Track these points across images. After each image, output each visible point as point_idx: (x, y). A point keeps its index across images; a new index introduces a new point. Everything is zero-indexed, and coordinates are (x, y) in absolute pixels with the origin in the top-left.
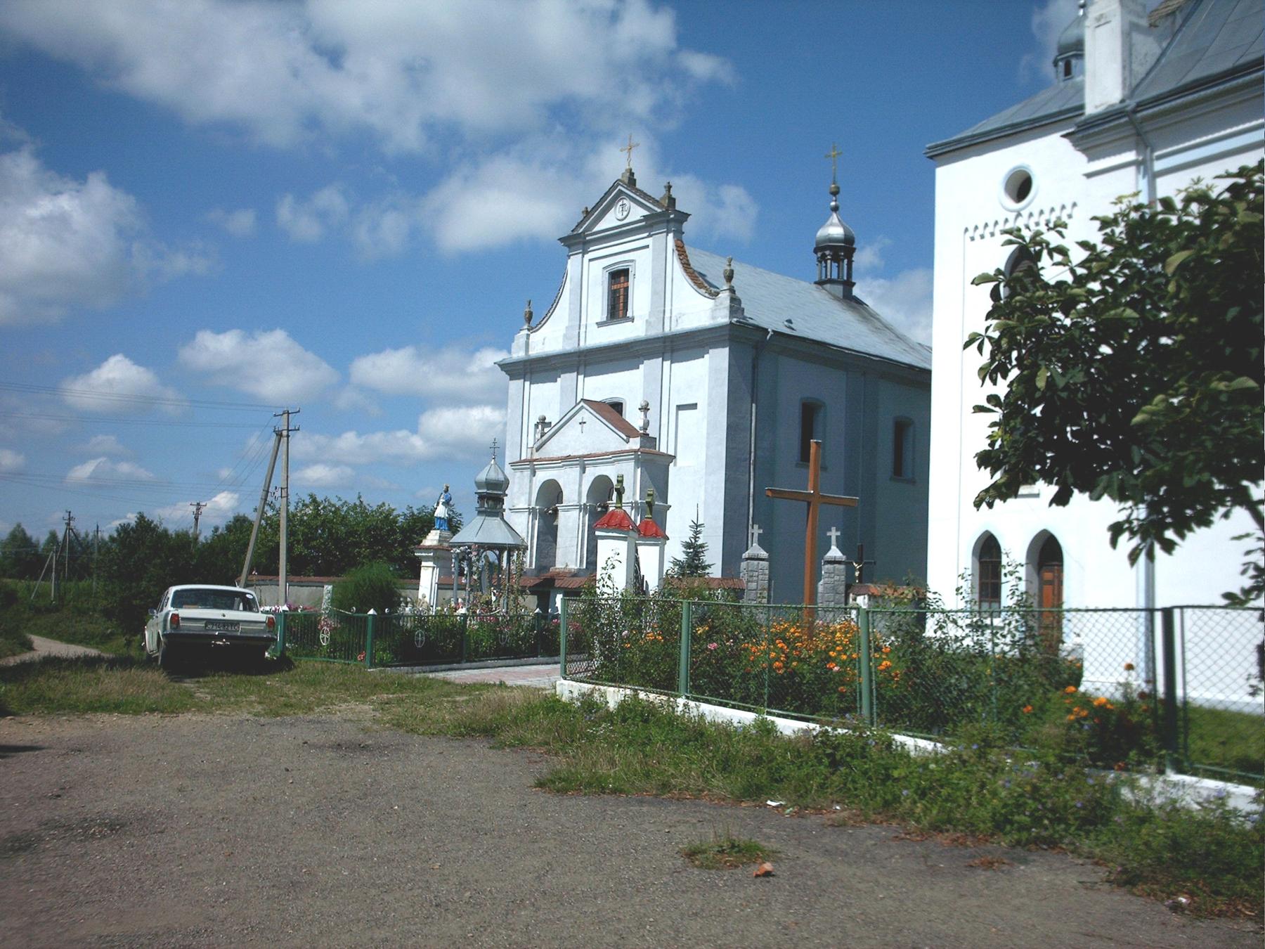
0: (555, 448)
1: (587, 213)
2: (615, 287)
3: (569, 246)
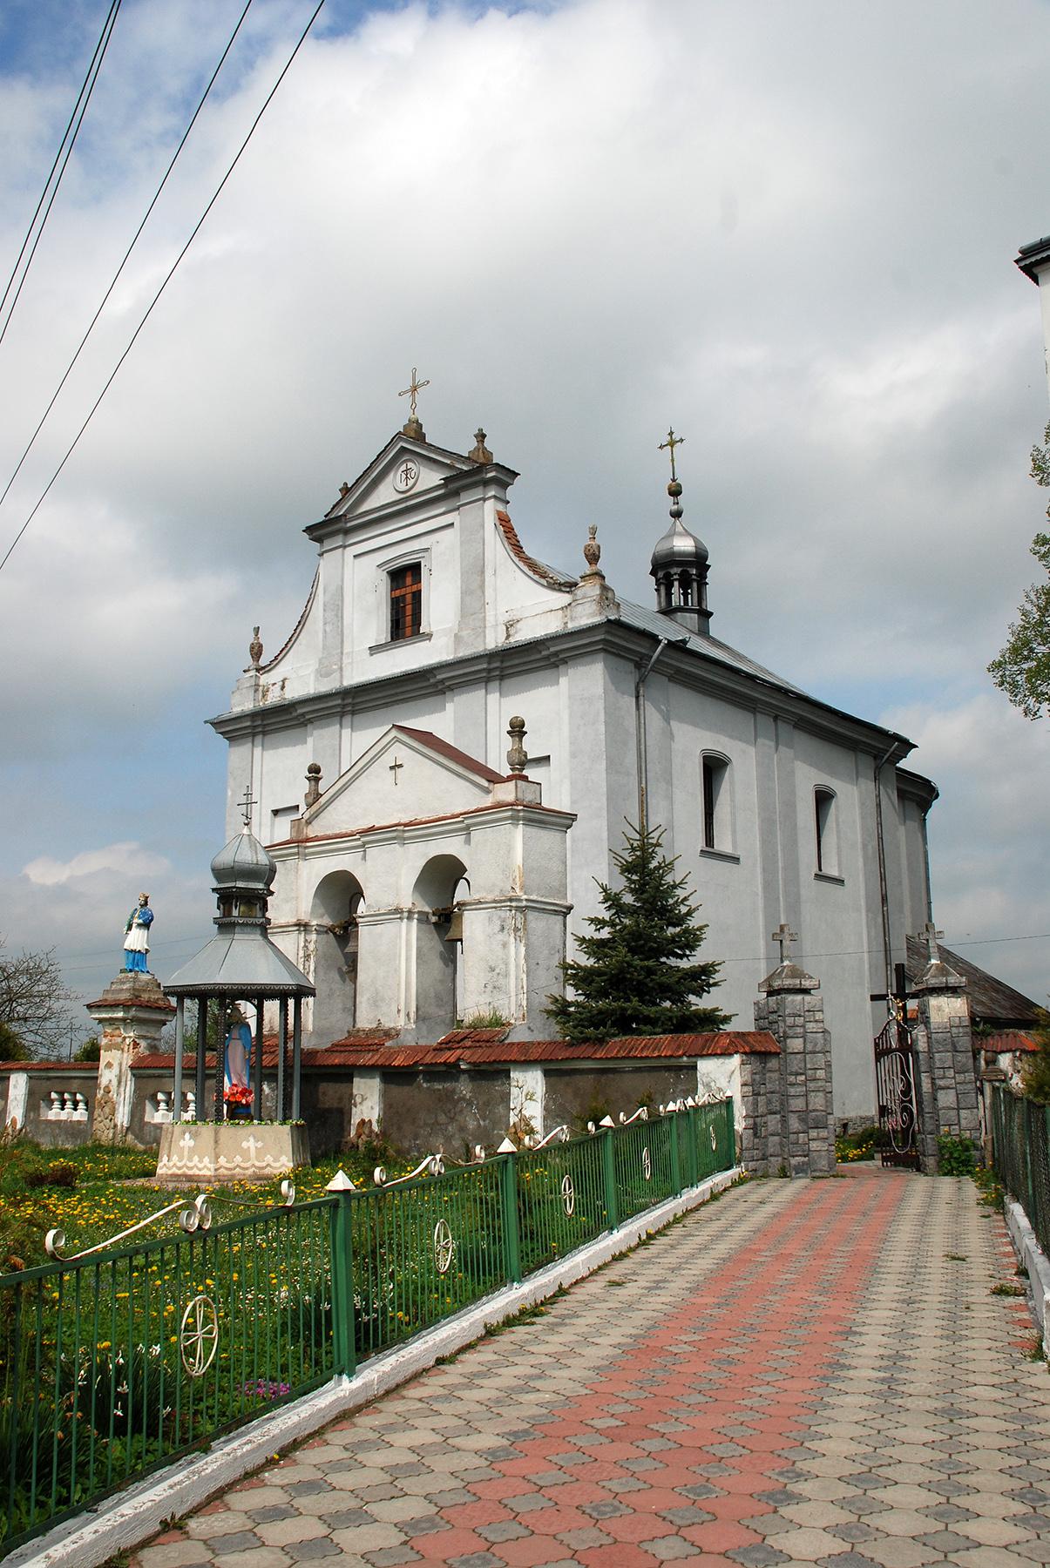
0: (342, 816)
1: (346, 490)
2: (398, 593)
3: (319, 540)
